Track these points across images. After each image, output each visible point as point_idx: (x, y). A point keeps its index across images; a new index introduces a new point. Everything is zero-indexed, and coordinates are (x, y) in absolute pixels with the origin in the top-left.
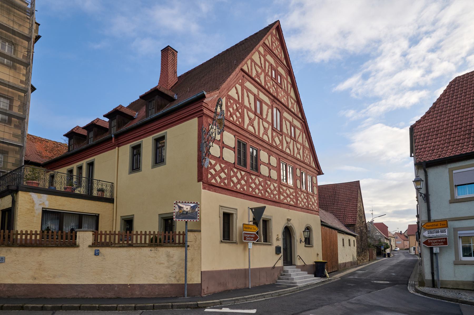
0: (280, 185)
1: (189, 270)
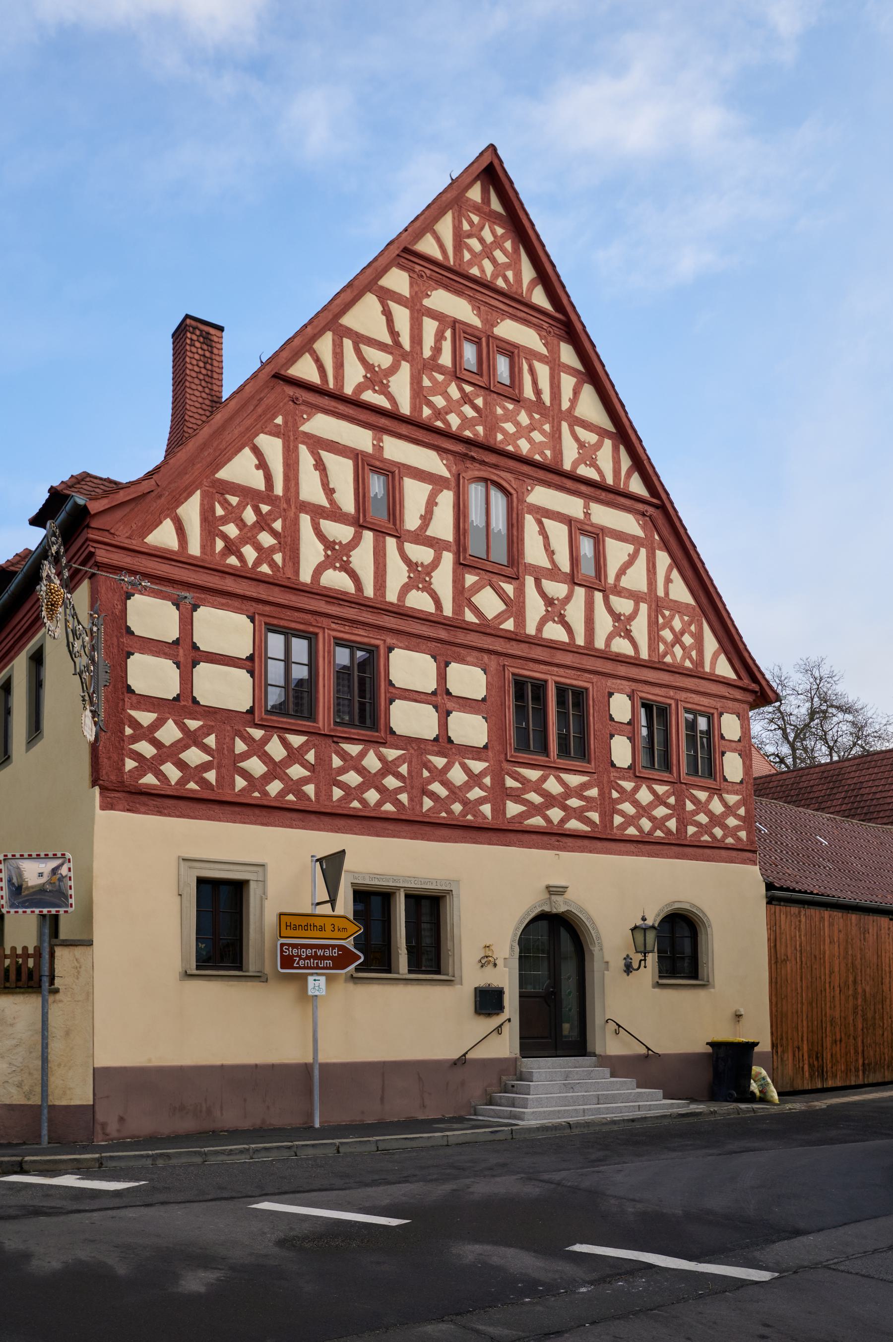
0: (506, 766)
1: (59, 1065)
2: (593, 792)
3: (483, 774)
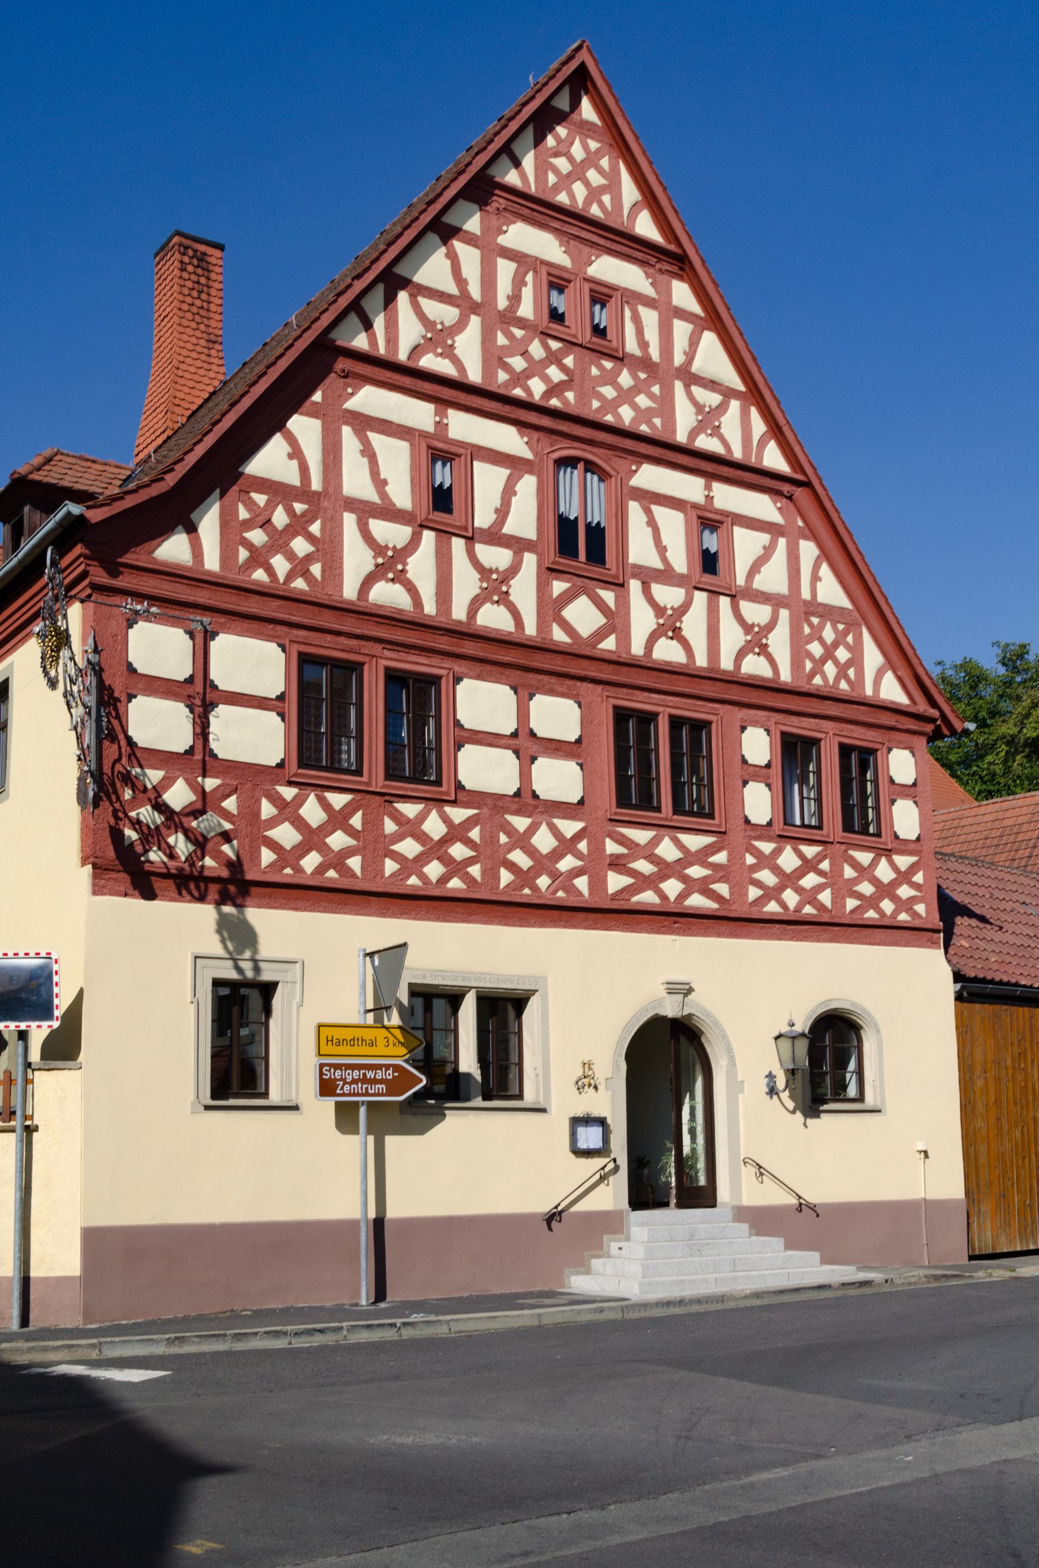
2: (721, 858)
3: (578, 837)
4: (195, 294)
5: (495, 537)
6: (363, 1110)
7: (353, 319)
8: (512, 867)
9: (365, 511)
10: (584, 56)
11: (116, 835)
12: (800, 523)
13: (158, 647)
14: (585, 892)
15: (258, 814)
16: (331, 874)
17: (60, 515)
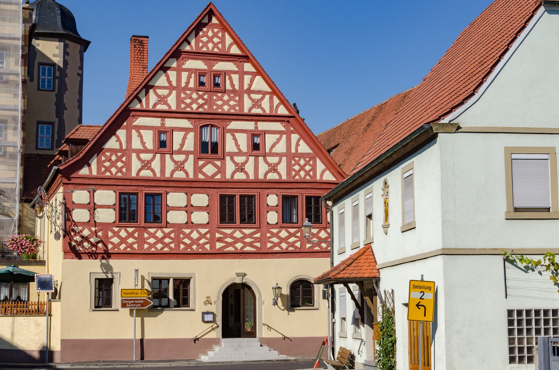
2: (258, 235)
3: (206, 233)
4: (139, 54)
5: (180, 152)
6: (134, 311)
7: (136, 100)
8: (184, 244)
9: (138, 152)
10: (211, 6)
11: (70, 244)
12: (292, 129)
13: (80, 196)
14: (208, 249)
15: (108, 236)
16: (129, 249)
17: (53, 170)
